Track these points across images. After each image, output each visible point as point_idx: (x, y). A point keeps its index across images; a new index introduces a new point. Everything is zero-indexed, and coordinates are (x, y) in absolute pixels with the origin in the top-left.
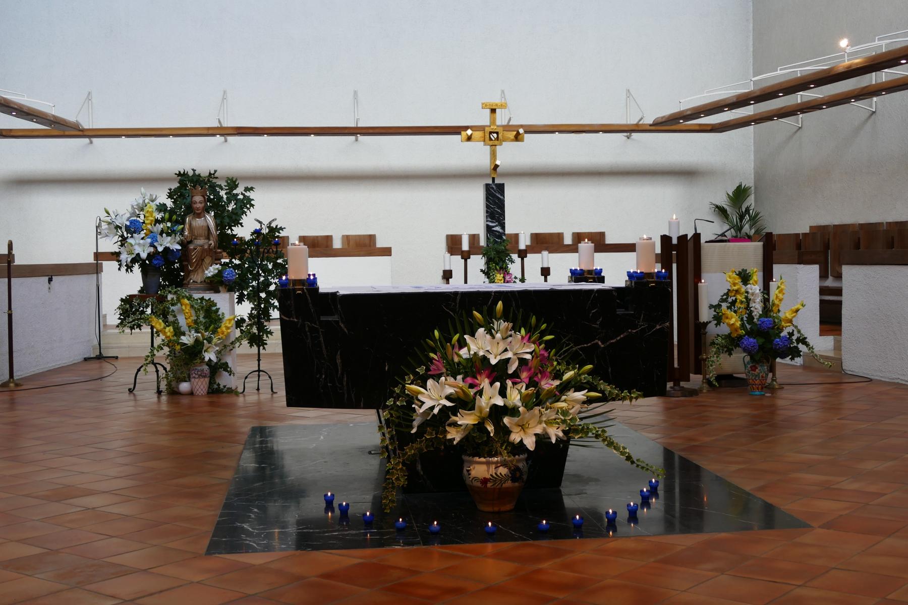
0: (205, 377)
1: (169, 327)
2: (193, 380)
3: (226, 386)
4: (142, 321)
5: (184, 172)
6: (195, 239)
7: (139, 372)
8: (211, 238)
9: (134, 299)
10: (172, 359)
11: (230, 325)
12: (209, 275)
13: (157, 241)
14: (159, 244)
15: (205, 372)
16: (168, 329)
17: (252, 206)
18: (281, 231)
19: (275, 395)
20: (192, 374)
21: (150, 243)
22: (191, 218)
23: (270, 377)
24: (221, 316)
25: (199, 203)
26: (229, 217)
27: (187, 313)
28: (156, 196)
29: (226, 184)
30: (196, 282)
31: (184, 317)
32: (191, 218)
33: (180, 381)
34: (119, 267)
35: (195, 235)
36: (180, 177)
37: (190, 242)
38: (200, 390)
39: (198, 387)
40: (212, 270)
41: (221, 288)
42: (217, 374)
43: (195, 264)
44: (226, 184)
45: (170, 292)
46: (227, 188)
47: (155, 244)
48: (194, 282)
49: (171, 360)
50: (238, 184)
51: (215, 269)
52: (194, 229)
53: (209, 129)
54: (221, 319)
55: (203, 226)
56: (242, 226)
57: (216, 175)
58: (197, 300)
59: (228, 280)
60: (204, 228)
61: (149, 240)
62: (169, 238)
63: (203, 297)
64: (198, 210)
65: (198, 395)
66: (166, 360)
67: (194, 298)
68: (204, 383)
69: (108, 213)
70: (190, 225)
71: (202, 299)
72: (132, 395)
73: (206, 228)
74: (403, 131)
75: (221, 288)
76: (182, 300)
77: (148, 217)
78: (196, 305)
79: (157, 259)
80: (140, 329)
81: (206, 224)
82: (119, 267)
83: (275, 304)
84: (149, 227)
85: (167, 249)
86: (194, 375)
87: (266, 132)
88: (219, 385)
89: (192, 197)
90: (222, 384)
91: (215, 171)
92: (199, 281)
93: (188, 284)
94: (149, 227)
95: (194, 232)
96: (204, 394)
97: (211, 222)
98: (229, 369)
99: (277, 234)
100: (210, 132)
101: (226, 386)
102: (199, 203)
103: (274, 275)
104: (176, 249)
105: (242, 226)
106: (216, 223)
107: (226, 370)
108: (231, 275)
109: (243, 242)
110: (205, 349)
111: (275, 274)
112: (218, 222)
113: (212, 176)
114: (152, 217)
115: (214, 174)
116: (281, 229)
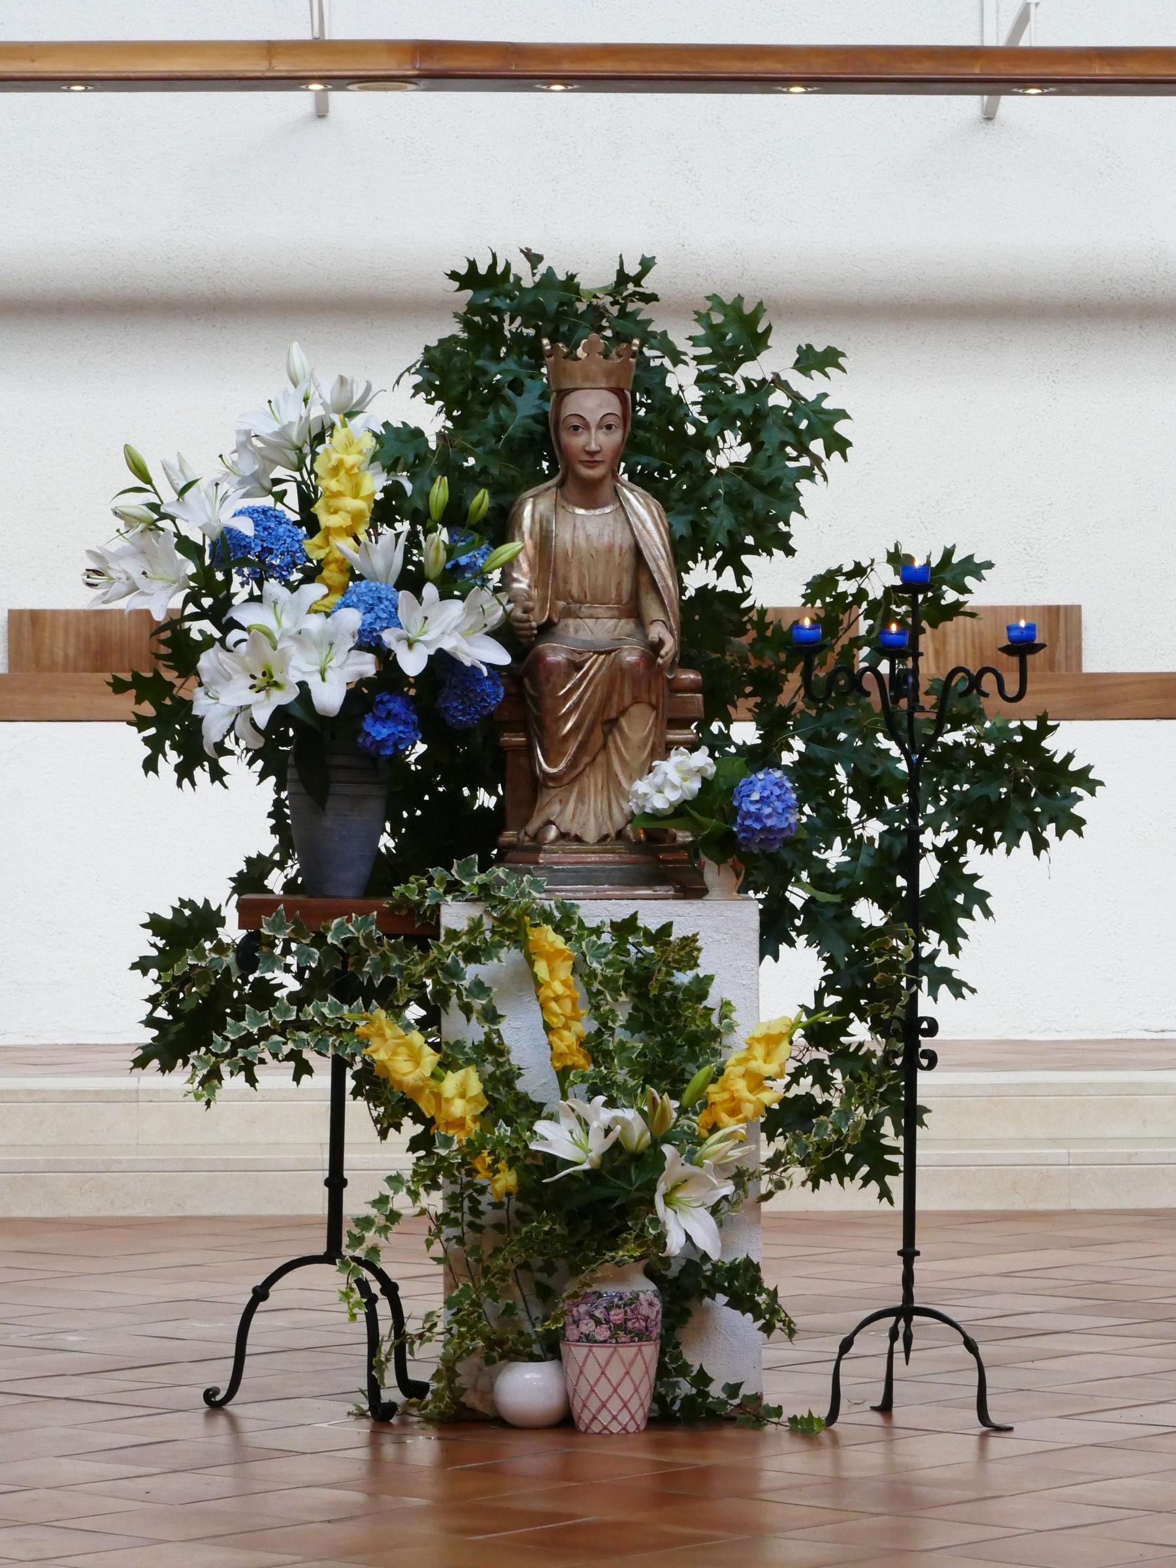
0: (641, 1336)
1: (461, 1072)
2: (578, 1352)
3: (738, 1386)
4: (304, 1035)
5: (493, 267)
6: (568, 613)
7: (262, 1306)
8: (653, 611)
9: (264, 919)
10: (460, 1240)
11: (770, 1069)
12: (660, 803)
13: (393, 620)
14: (399, 639)
15: (644, 1310)
16: (451, 1082)
17: (838, 445)
18: (969, 581)
19: (997, 1444)
20: (576, 1322)
21: (361, 632)
22: (545, 505)
23: (971, 1346)
24: (714, 1019)
25: (599, 427)
26: (737, 502)
27: (557, 999)
28: (368, 388)
29: (699, 331)
30: (578, 839)
31: (537, 1018)
32: (545, 505)
33: (502, 1358)
34: (148, 751)
35: (568, 597)
36: (469, 294)
37: (547, 629)
38: (615, 1405)
39: (603, 1389)
40: (675, 777)
41: (711, 873)
42: (693, 1321)
43: (572, 749)
44: (699, 331)
45: (453, 887)
46: (707, 350)
47: (389, 637)
48: (563, 836)
49: (453, 1245)
50: (769, 330)
51: (687, 774)
52: (566, 561)
53: (271, 48)
54: (716, 1035)
55: (610, 549)
56: (790, 552)
57: (649, 285)
58: (598, 931)
59: (765, 829)
60: (617, 552)
61: (352, 618)
62: (455, 608)
63: (634, 917)
64: (592, 464)
65: (605, 1434)
66: (429, 1243)
67: (581, 924)
68: (638, 1371)
69: (140, 471)
70: (544, 542)
71: (626, 928)
72: (221, 1422)
73: (628, 560)
74: (667, 69)
75: (711, 873)
76: (533, 934)
77: (338, 495)
78: (597, 958)
79: (390, 715)
80: (252, 1080)
81: (627, 541)
82: (148, 751)
83: (939, 963)
84: (345, 545)
85: (442, 662)
86: (587, 1326)
87: (567, 68)
88: (703, 1379)
89: (563, 394)
90: (721, 1375)
91: (647, 264)
92: (591, 835)
93: (538, 850)
94: (345, 545)
95: (566, 581)
96: (632, 1428)
97: (650, 525)
98: (762, 1299)
99: (950, 596)
100: (282, 67)
101: (738, 1386)
102: (599, 427)
103: (939, 811)
104: (490, 666)
105: (790, 552)
106: (670, 532)
107: (741, 1302)
108: (779, 805)
109: (769, 633)
110: (662, 1187)
111: (944, 801)
112: (682, 529)
113: (631, 286)
114: (356, 496)
115: (637, 280)
116: (973, 568)
